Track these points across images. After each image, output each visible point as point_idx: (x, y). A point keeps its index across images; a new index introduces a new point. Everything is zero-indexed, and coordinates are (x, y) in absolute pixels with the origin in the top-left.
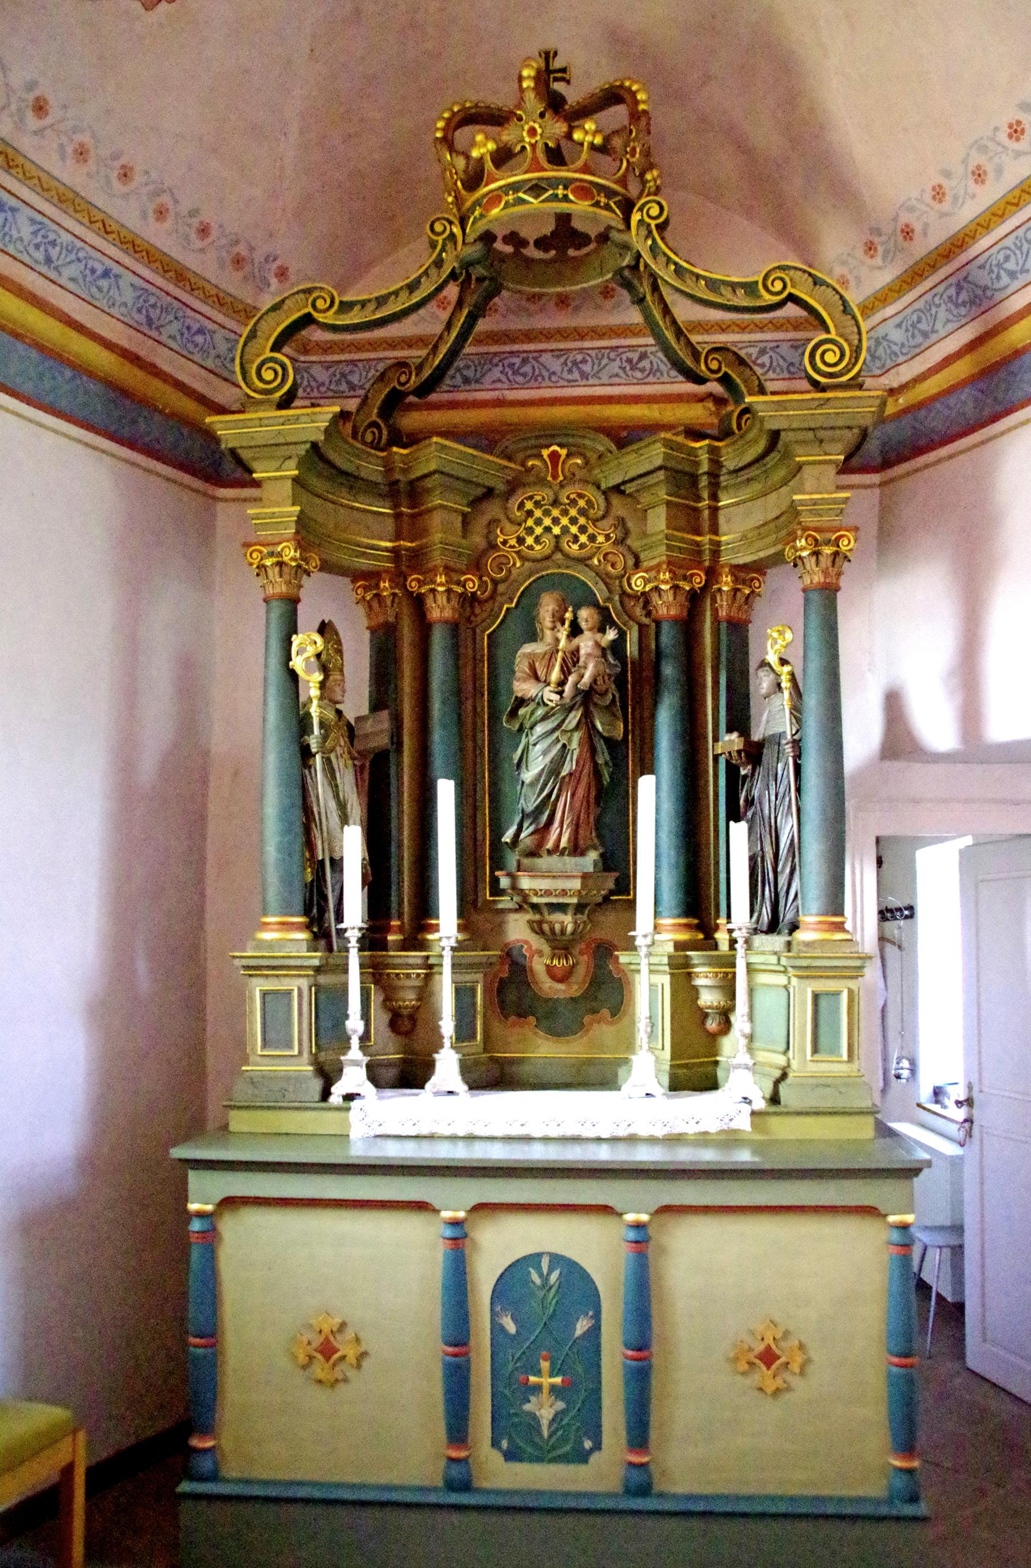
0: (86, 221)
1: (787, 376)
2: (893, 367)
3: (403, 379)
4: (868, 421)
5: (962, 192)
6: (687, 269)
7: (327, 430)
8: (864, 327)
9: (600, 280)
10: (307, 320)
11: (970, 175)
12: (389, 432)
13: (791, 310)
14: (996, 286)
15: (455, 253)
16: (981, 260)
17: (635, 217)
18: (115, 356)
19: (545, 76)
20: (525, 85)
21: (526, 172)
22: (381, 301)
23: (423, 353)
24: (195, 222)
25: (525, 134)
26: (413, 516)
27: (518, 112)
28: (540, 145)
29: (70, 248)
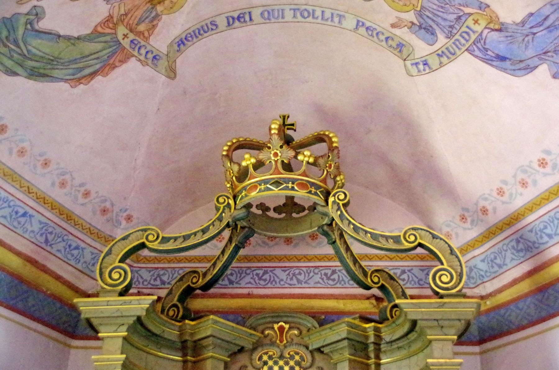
0: (18, 186)
1: (419, 286)
2: (482, 283)
3: (195, 280)
4: (470, 317)
6: (359, 228)
7: (147, 310)
8: (463, 260)
9: (310, 231)
10: (143, 246)
11: (518, 184)
12: (184, 311)
13: (419, 250)
14: (541, 241)
15: (229, 214)
16: (529, 228)
17: (331, 199)
18: (21, 260)
19: (283, 128)
20: (273, 132)
21: (271, 175)
22: (186, 238)
23: (208, 265)
24: (82, 189)
25: (272, 155)
26: (195, 362)
27: (269, 145)
28: (279, 162)
29: (5, 200)
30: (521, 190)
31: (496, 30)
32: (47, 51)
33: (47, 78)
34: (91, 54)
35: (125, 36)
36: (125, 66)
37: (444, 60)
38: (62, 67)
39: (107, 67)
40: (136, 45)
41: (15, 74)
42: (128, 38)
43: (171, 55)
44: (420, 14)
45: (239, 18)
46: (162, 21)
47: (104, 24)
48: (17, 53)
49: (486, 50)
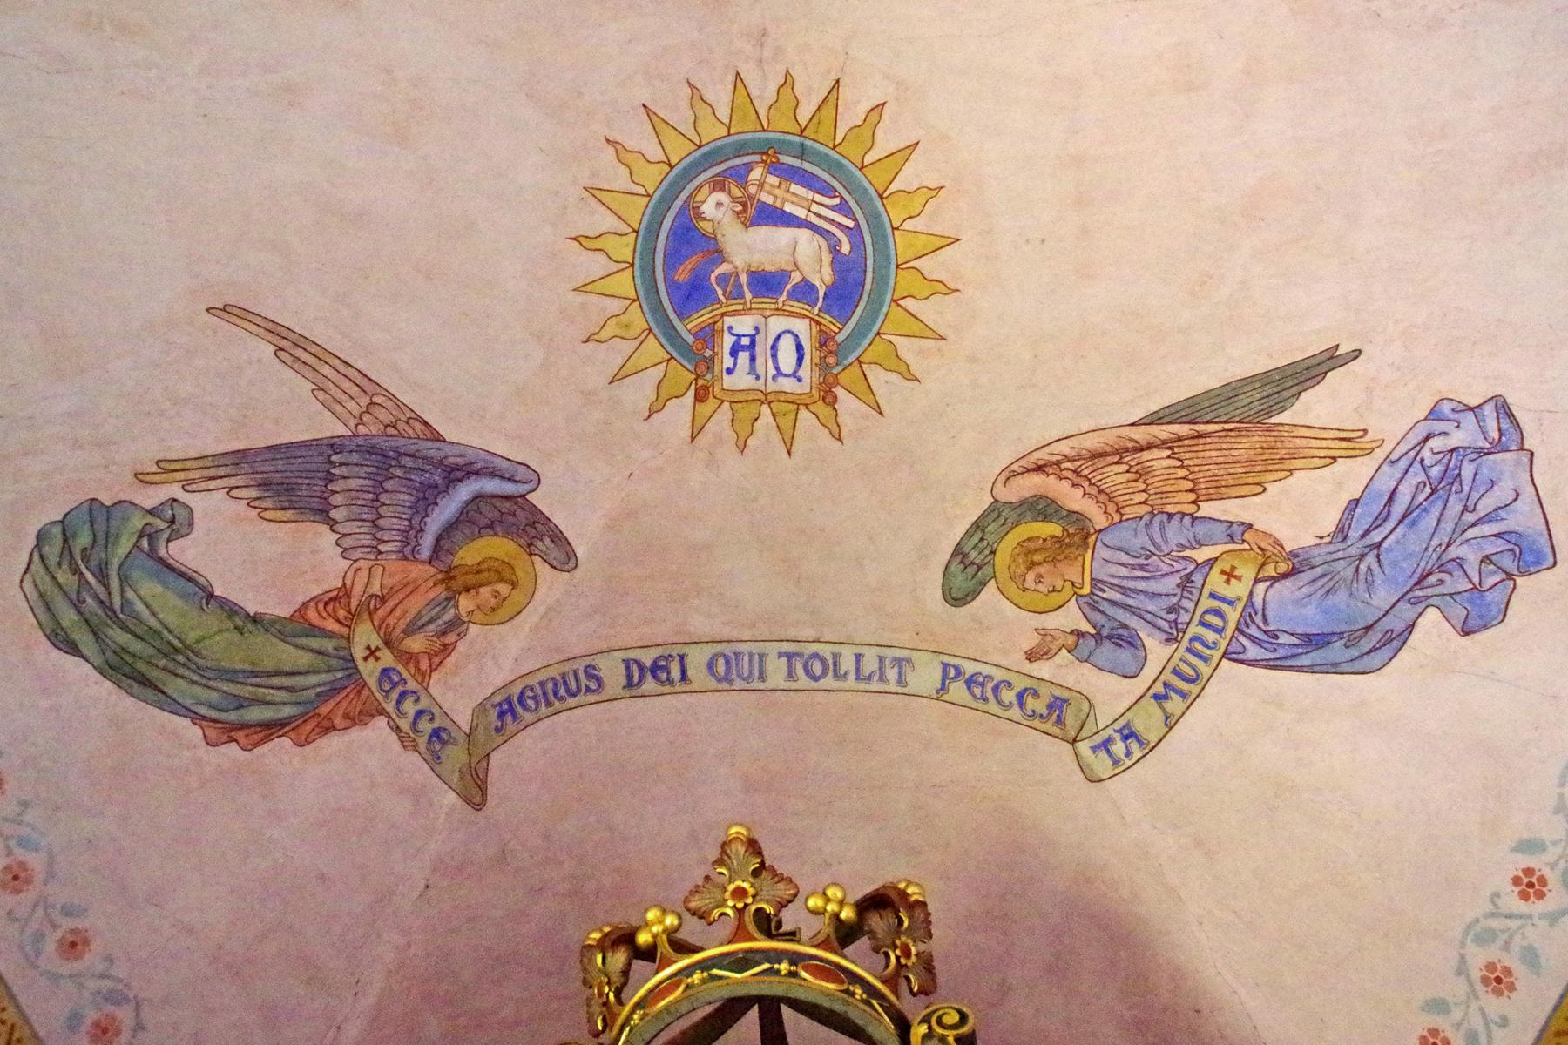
5: (1478, 1025)
30: (1494, 1005)
31: (1285, 576)
32: (171, 619)
33: (150, 693)
34: (277, 674)
35: (372, 653)
36: (356, 734)
37: (1175, 704)
38: (195, 678)
39: (309, 724)
40: (395, 685)
41: (73, 649)
42: (377, 659)
43: (480, 735)
44: (1091, 605)
45: (655, 669)
46: (468, 638)
47: (326, 604)
48: (96, 597)
49: (1274, 635)
